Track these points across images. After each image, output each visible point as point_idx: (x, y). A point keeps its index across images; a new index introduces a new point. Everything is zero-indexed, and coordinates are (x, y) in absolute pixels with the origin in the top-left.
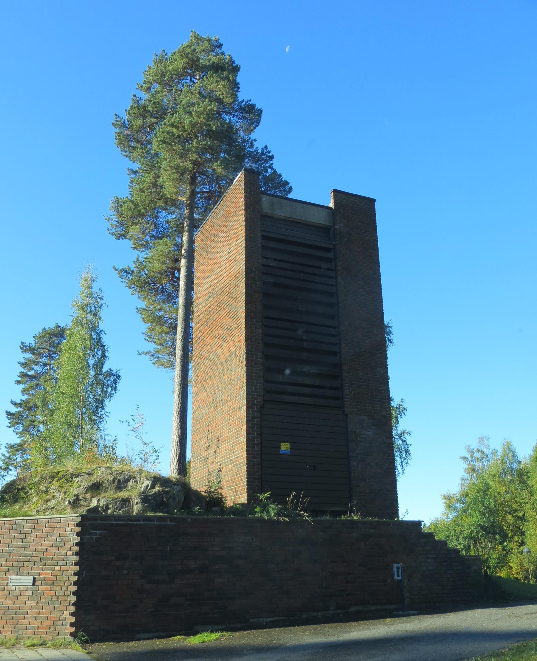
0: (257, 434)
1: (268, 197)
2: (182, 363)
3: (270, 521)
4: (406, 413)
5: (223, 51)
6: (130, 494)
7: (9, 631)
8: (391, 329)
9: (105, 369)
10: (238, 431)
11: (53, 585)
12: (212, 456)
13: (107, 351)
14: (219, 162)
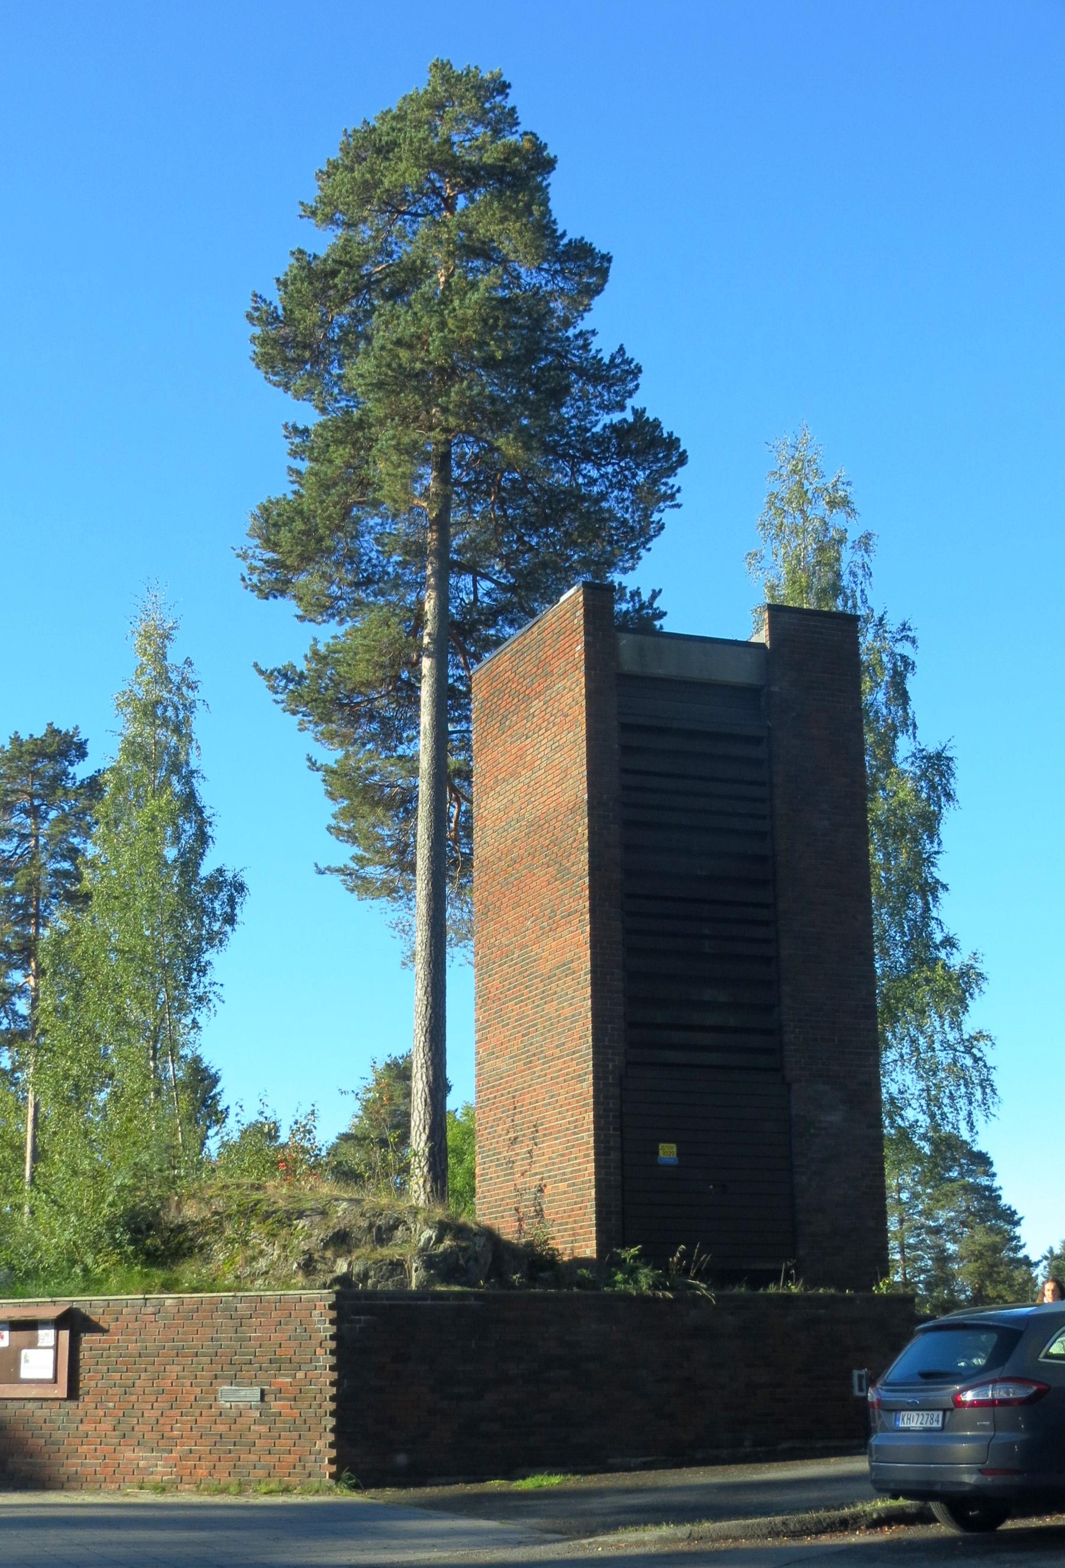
0: (615, 1129)
1: (631, 637)
5: (513, 109)
8: (951, 764)
9: (206, 869)
10: (576, 1121)
13: (210, 823)
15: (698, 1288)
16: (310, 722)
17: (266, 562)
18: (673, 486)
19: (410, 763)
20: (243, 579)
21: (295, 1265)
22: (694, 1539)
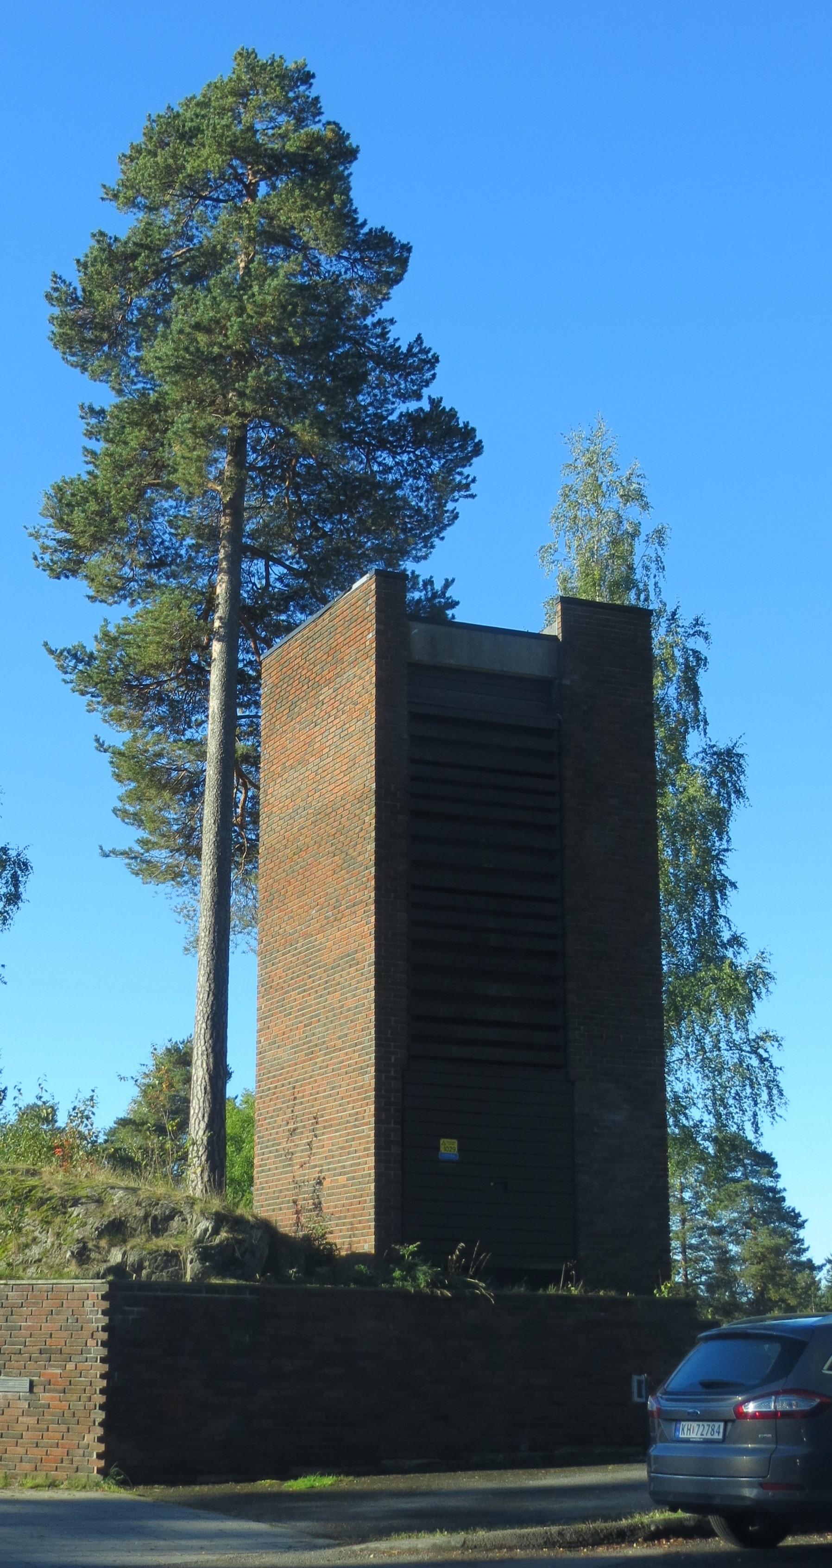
2: (215, 900)
3: (419, 1296)
4: (771, 986)
6: (176, 1242)
8: (742, 761)
10: (357, 1113)
11: (64, 1392)
12: (302, 1151)
15: (476, 1286)
16: (98, 703)
17: (59, 541)
18: (468, 476)
19: (198, 748)
20: (35, 558)
21: (69, 1254)
22: (468, 1548)
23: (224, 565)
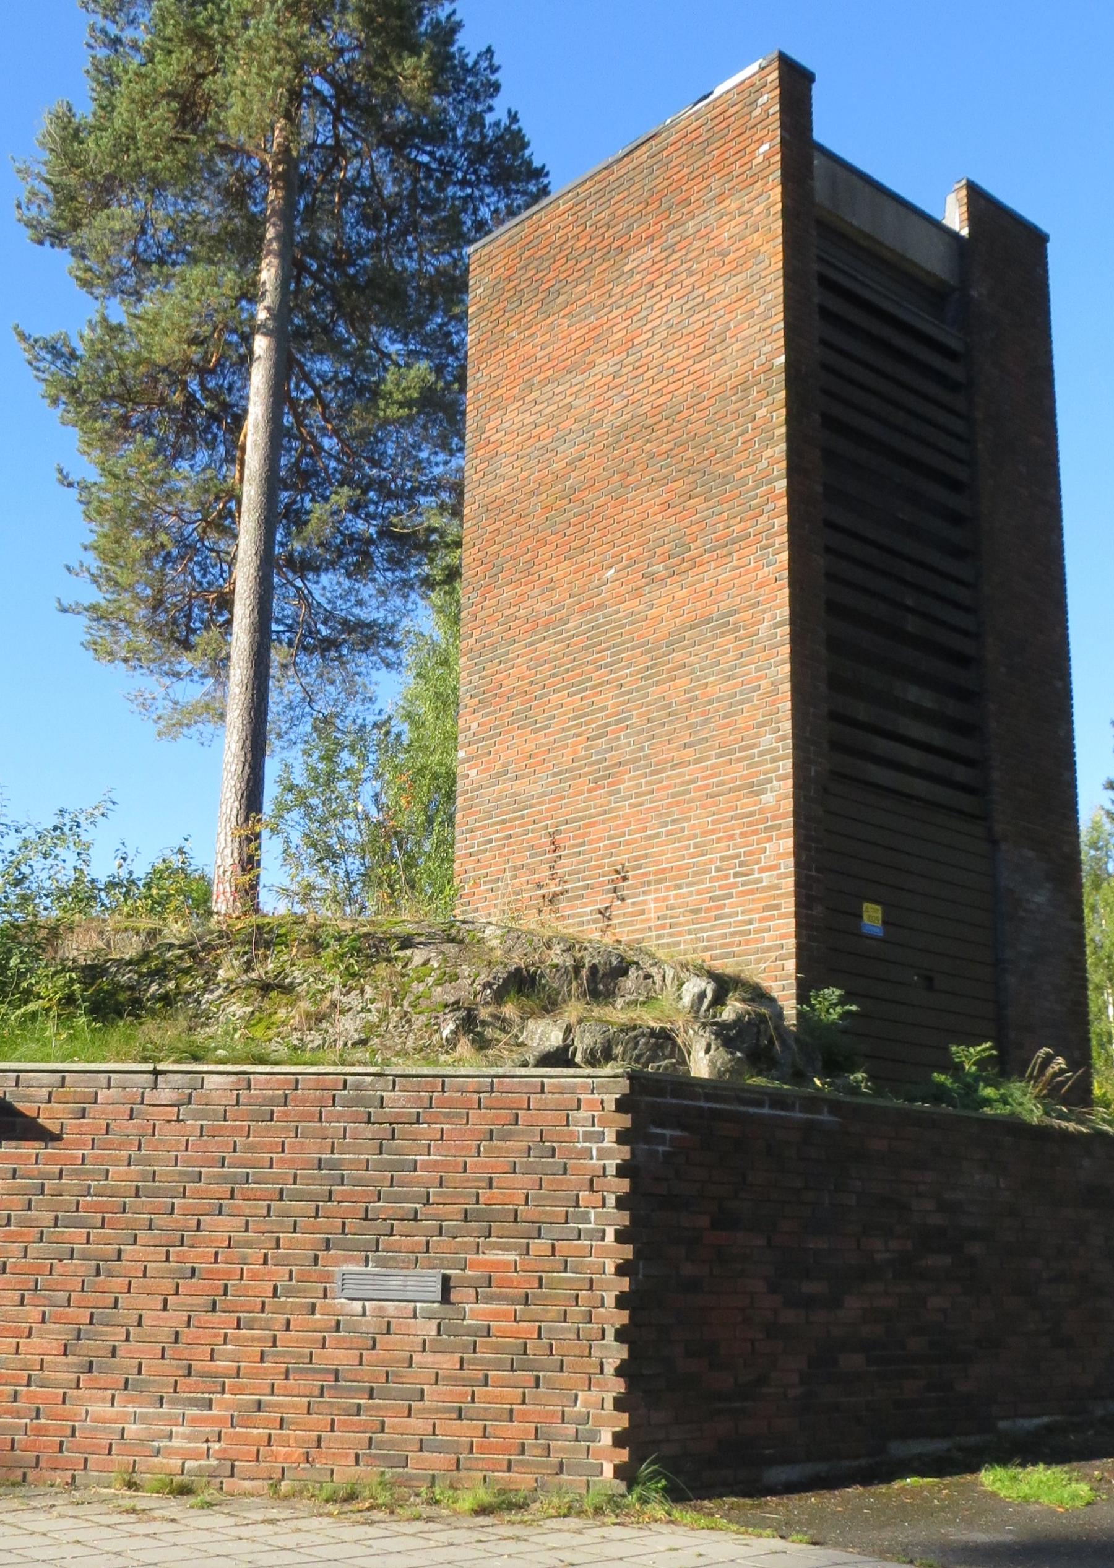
2: (255, 649)
7: (347, 1455)
11: (526, 1304)
14: (425, 56)
23: (275, 246)
